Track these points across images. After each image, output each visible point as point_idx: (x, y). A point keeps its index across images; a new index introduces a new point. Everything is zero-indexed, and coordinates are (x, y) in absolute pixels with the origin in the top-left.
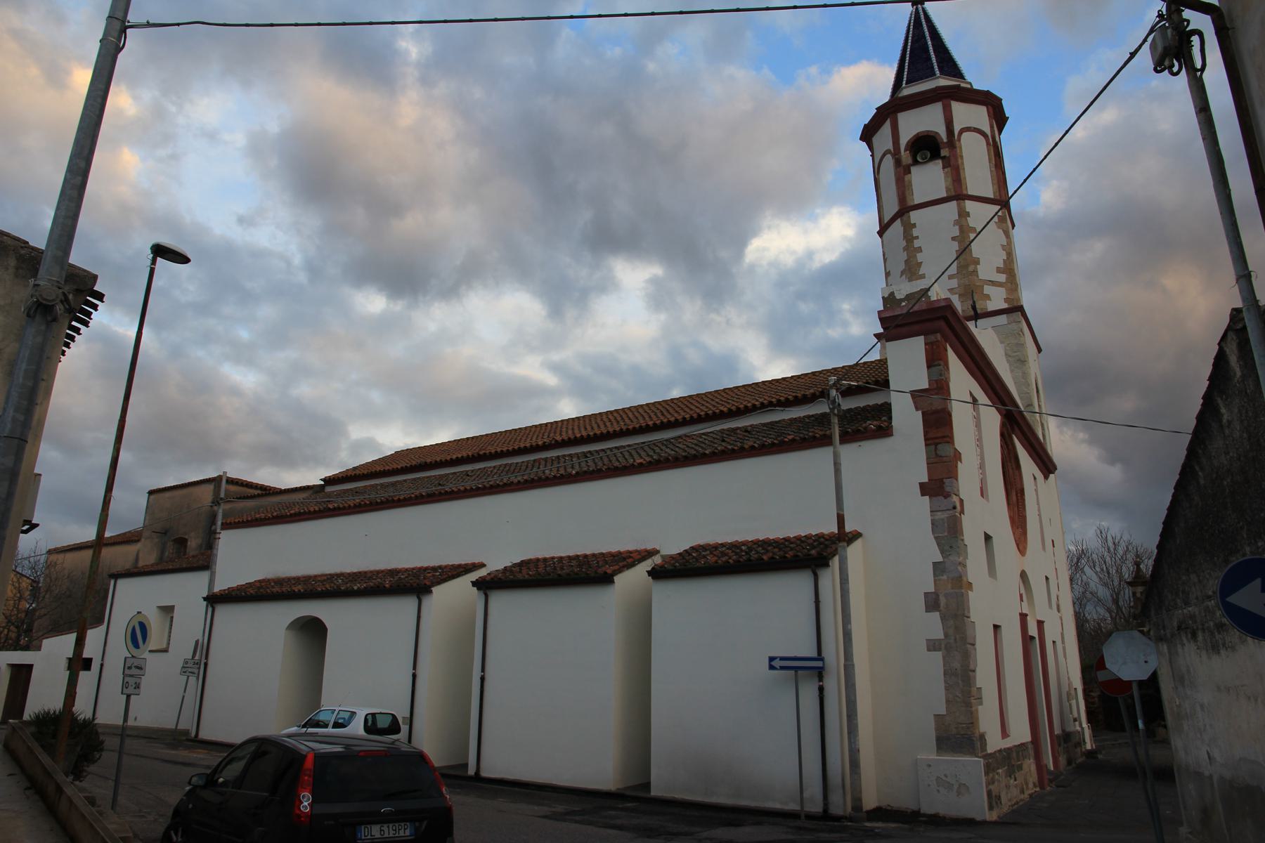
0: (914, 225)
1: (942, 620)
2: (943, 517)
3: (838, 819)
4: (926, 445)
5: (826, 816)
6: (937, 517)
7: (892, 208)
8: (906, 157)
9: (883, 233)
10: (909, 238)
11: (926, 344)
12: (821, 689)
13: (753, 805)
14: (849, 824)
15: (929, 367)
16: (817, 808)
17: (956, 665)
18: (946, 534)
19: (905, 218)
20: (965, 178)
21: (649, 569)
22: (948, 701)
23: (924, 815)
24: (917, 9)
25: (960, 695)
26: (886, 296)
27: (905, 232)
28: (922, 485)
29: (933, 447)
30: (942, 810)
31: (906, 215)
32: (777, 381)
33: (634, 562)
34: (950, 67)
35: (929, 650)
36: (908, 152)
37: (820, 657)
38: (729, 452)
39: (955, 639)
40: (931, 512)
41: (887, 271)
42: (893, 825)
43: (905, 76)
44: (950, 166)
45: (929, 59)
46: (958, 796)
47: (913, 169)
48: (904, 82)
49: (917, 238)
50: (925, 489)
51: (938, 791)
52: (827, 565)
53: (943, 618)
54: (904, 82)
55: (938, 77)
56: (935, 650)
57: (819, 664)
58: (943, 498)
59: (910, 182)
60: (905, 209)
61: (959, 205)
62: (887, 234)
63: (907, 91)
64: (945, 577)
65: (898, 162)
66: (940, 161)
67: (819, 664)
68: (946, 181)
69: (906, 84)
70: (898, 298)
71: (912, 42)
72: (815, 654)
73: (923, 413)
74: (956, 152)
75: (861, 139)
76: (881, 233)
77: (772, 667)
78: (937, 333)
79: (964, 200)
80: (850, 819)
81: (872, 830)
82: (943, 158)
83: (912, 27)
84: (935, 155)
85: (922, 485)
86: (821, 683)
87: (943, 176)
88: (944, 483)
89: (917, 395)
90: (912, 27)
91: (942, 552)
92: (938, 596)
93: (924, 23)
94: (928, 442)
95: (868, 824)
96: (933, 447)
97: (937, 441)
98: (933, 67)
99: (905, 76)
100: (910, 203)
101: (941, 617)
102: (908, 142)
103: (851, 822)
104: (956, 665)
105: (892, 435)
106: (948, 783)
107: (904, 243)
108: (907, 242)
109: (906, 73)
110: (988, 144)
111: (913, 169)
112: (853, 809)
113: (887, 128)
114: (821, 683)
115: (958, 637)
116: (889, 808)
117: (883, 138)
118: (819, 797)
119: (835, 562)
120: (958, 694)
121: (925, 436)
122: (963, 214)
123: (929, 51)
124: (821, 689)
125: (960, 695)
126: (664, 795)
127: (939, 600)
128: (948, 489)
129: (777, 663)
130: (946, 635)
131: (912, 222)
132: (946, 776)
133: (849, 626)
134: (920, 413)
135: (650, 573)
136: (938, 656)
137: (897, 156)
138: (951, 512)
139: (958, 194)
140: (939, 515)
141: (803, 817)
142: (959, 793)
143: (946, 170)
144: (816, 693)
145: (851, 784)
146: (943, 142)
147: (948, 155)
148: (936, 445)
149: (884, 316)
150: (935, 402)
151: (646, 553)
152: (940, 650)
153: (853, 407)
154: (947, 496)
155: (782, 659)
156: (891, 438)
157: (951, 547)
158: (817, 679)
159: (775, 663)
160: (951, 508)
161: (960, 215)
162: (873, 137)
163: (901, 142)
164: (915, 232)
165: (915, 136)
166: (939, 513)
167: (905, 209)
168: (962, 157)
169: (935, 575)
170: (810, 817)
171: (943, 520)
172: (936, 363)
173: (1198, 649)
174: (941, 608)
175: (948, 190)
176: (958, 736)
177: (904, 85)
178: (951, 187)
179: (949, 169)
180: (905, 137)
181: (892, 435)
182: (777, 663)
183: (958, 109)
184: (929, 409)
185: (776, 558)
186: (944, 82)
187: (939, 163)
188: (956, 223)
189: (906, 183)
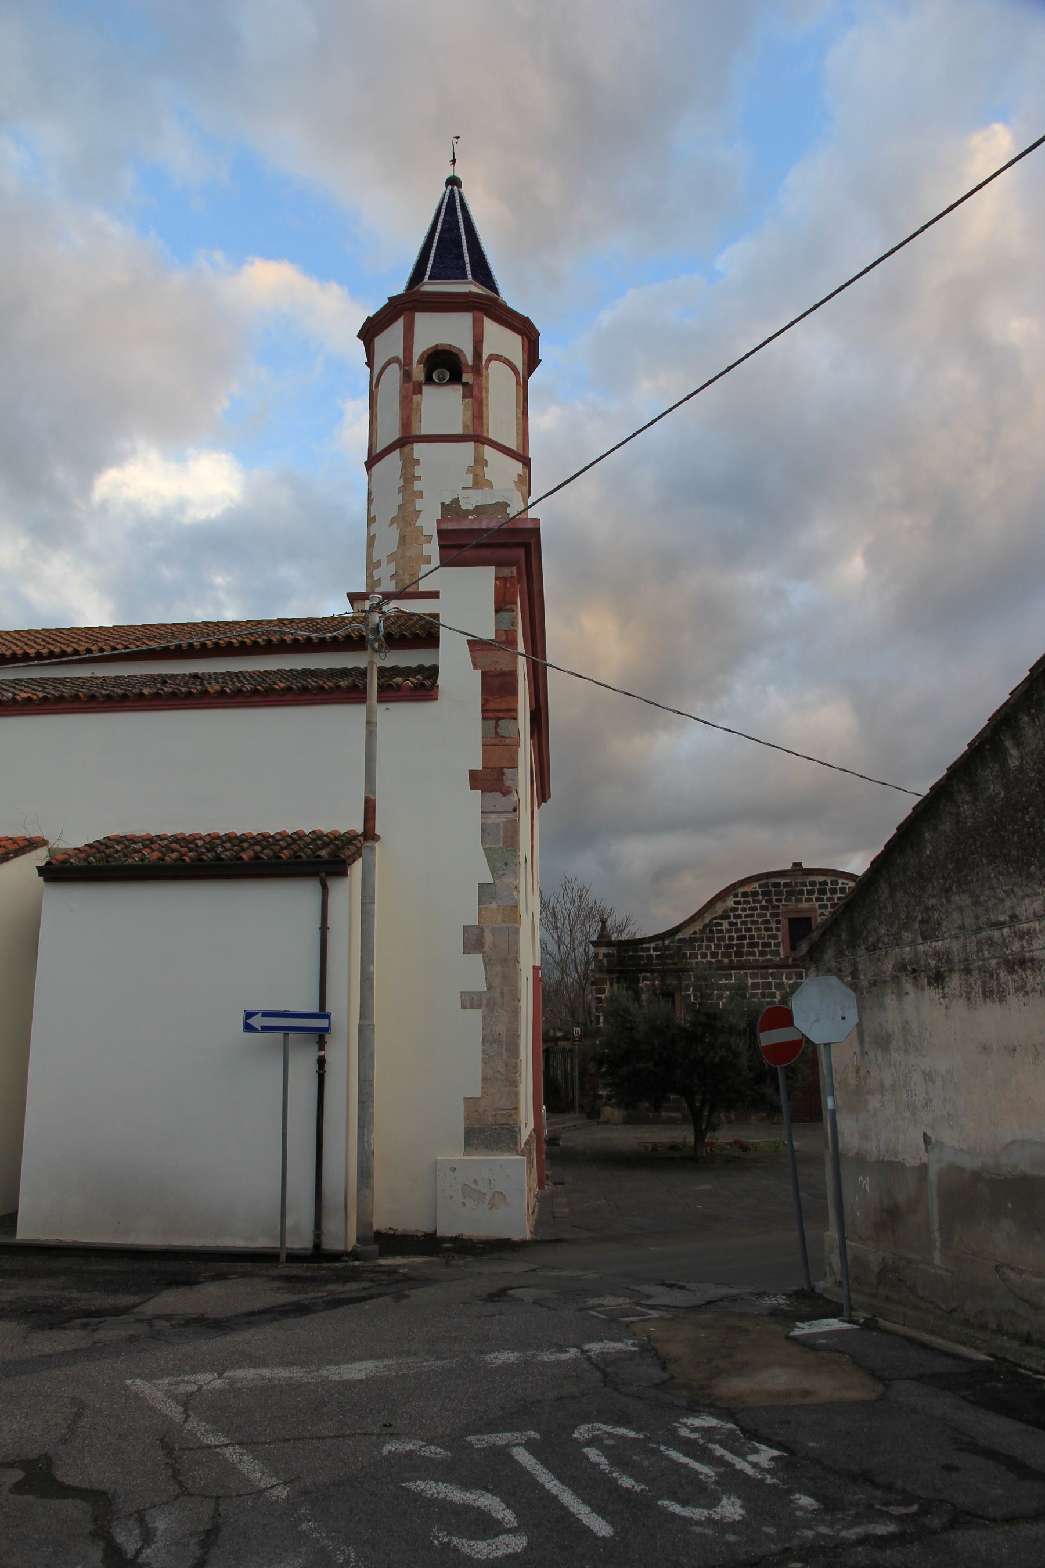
0: (417, 462)
1: (485, 966)
2: (498, 820)
3: (336, 1257)
4: (484, 719)
5: (318, 1254)
6: (489, 821)
7: (390, 433)
8: (418, 372)
9: (373, 465)
10: (408, 477)
11: (496, 579)
12: (321, 1062)
13: (197, 1245)
14: (357, 1263)
15: (497, 611)
16: (301, 1240)
17: (501, 1028)
18: (501, 845)
19: (406, 449)
20: (487, 417)
21: (42, 864)
22: (485, 1079)
23: (444, 1240)
24: (452, 191)
25: (502, 1070)
26: (447, 502)
27: (404, 467)
28: (473, 774)
29: (492, 723)
30: (468, 1231)
31: (409, 446)
32: (227, 624)
33: (8, 853)
34: (483, 274)
35: (464, 1007)
36: (422, 366)
37: (323, 1013)
38: (183, 696)
39: (502, 994)
40: (482, 812)
41: (372, 516)
42: (419, 1260)
43: (429, 269)
44: (472, 397)
45: (463, 258)
46: (490, 1209)
47: (425, 389)
48: (427, 276)
49: (419, 478)
50: (476, 780)
51: (464, 1204)
52: (343, 874)
53: (488, 963)
54: (427, 276)
55: (470, 283)
56: (472, 1007)
57: (322, 1023)
58: (501, 795)
59: (419, 405)
60: (406, 440)
61: (476, 448)
62: (379, 467)
63: (429, 287)
64: (494, 906)
65: (407, 376)
66: (460, 388)
67: (322, 1023)
68: (464, 415)
69: (430, 279)
70: (464, 507)
71: (442, 230)
72: (315, 1009)
73: (484, 674)
74: (482, 381)
75: (359, 336)
76: (369, 465)
77: (248, 1028)
78: (514, 566)
79: (483, 443)
80: (354, 1255)
81: (392, 1271)
82: (465, 385)
83: (443, 211)
84: (456, 378)
85: (473, 774)
86: (322, 1053)
87: (461, 407)
88: (503, 774)
89: (476, 645)
90: (443, 211)
91: (493, 871)
92: (482, 931)
93: (459, 210)
94: (486, 715)
95: (382, 1261)
96: (492, 723)
97: (500, 715)
98: (465, 269)
99: (429, 269)
100: (416, 432)
101: (484, 961)
102: (424, 353)
103: (358, 1260)
104: (501, 1028)
105: (437, 699)
106: (479, 1192)
107: (401, 483)
108: (405, 480)
109: (430, 266)
110: (518, 383)
111: (425, 389)
112: (359, 1240)
113: (398, 328)
114: (322, 1053)
115: (506, 989)
116: (392, 1232)
117: (391, 341)
118: (308, 1226)
119: (356, 869)
120: (499, 1069)
121: (483, 706)
122: (480, 462)
123: (461, 247)
124: (321, 1062)
125: (502, 1070)
126: (42, 1237)
127: (483, 937)
128: (508, 783)
129: (257, 1021)
130: (489, 987)
131: (415, 457)
132: (476, 1182)
133: (372, 967)
134: (479, 673)
135: (41, 871)
136: (476, 1016)
137: (406, 368)
138: (510, 815)
139: (476, 436)
140: (493, 819)
141: (283, 1258)
142: (492, 1206)
143: (466, 400)
144: (314, 1066)
145: (359, 1201)
146: (467, 365)
147: (471, 383)
148: (498, 719)
149: (445, 528)
150: (500, 662)
151: (26, 843)
152: (479, 1007)
153: (350, 667)
154: (506, 792)
155: (266, 1014)
156: (434, 703)
157: (506, 864)
158: (316, 1047)
159: (254, 1021)
160: (511, 810)
161: (475, 461)
162: (375, 337)
163: (414, 350)
164: (417, 471)
165: (433, 347)
166: (493, 816)
167: (406, 440)
168: (487, 389)
169: (480, 901)
170: (294, 1257)
171: (498, 825)
172: (508, 606)
173: (944, 997)
174: (486, 948)
175: (465, 426)
176: (496, 1127)
177: (426, 280)
178: (470, 423)
179: (470, 400)
180: (421, 346)
181: (437, 699)
182: (257, 1021)
183: (491, 328)
184: (493, 669)
185: (262, 859)
186: (475, 288)
187: (459, 390)
188: (470, 470)
189: (415, 405)
